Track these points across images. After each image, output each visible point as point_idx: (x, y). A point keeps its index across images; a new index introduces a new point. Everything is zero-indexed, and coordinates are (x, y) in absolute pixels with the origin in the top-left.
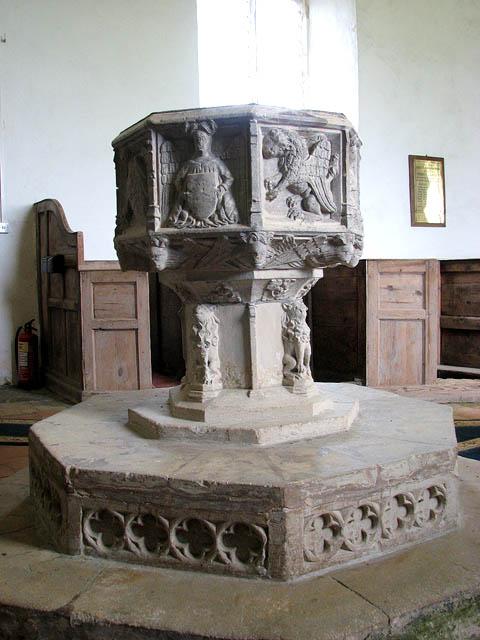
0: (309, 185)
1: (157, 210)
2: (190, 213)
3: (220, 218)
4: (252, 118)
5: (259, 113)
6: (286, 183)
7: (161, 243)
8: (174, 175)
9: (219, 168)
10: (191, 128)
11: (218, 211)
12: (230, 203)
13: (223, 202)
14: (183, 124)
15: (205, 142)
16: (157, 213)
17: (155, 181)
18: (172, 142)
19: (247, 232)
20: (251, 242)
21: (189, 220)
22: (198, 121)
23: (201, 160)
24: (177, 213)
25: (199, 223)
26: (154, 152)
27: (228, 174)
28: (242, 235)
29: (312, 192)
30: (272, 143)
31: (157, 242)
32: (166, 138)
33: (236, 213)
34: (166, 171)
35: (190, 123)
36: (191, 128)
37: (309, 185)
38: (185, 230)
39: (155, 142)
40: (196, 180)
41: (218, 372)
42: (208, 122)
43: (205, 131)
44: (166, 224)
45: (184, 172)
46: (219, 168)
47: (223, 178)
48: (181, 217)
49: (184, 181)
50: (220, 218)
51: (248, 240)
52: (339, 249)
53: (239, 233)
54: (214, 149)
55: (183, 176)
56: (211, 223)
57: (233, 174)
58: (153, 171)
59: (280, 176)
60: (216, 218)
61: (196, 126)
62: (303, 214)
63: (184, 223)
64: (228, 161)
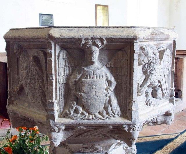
0: (159, 82)
1: (55, 104)
2: (83, 107)
3: (107, 113)
4: (136, 39)
5: (55, 33)
6: (149, 83)
7: (59, 130)
8: (68, 77)
9: (106, 75)
10: (86, 43)
11: (106, 108)
12: (114, 101)
13: (110, 102)
14: (80, 40)
15: (96, 51)
16: (56, 107)
17: (54, 81)
18: (67, 51)
19: (129, 125)
20: (131, 131)
21: (83, 114)
22: (92, 39)
23: (92, 68)
24: (72, 108)
25: (91, 117)
26: (53, 59)
27: (112, 79)
28: (125, 126)
29: (160, 86)
30: (144, 56)
31: (57, 129)
32: (63, 48)
33: (119, 109)
34: (62, 73)
35: (85, 39)
36: (86, 43)
37: (159, 82)
38: (79, 121)
39: (55, 51)
40: (90, 85)
41: (71, 94)
42: (101, 40)
43: (97, 45)
44: (64, 115)
45: (79, 77)
46: (106, 75)
47: (109, 83)
48: (76, 111)
49: (79, 85)
50: (107, 113)
51: (129, 130)
52: (168, 117)
53: (122, 125)
54: (100, 59)
55: (77, 80)
56: (100, 117)
57: (116, 79)
58: (52, 74)
59: (144, 77)
60: (105, 113)
61: (90, 42)
62: (150, 100)
63: (79, 115)
64: (113, 70)
